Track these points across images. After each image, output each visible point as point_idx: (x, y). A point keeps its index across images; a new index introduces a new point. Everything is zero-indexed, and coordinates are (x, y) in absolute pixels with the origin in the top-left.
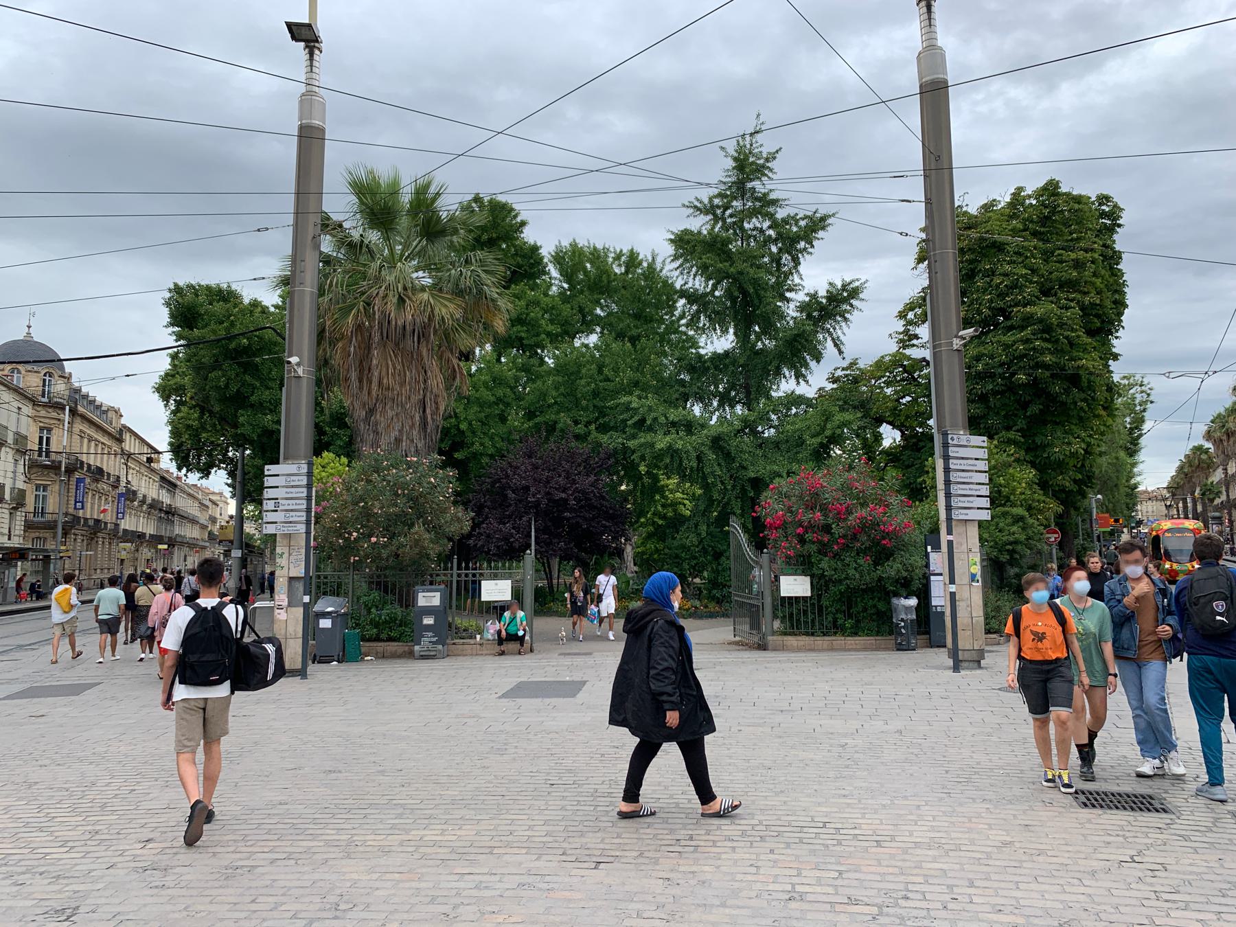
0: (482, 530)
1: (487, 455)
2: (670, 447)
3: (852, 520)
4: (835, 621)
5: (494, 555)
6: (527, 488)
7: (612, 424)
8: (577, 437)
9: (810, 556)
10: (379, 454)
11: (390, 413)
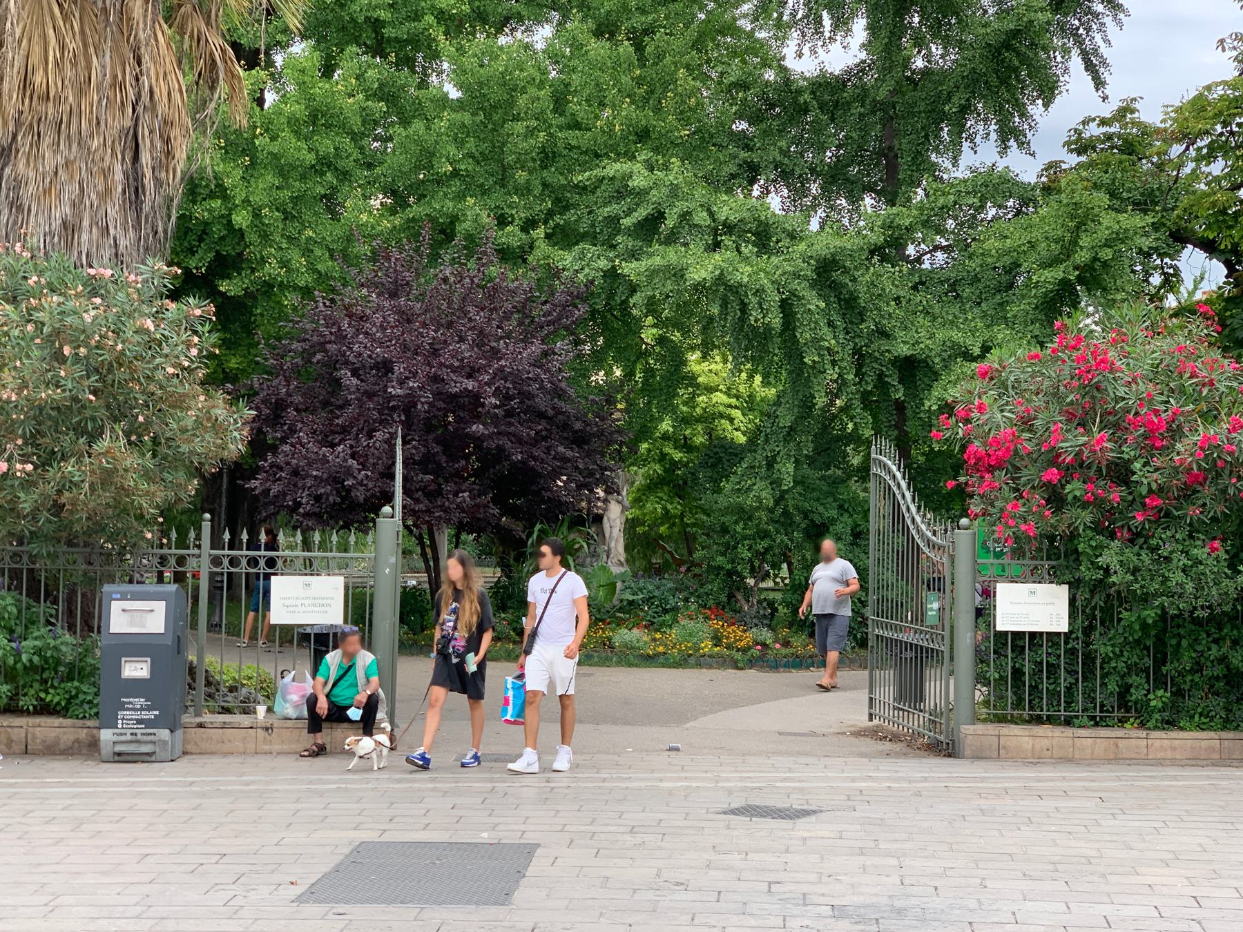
0: (280, 459)
1: (296, 288)
2: (720, 280)
3: (1185, 450)
4: (1125, 690)
5: (307, 515)
6: (385, 367)
7: (583, 227)
8: (505, 254)
9: (1073, 536)
10: (18, 257)
11: (50, 160)
